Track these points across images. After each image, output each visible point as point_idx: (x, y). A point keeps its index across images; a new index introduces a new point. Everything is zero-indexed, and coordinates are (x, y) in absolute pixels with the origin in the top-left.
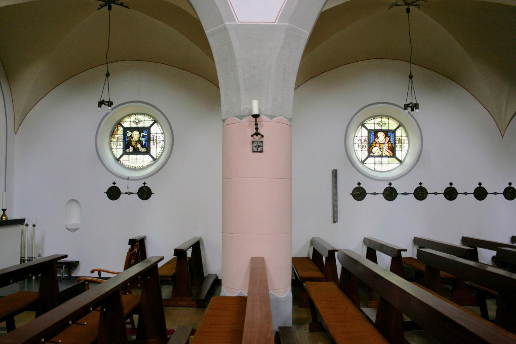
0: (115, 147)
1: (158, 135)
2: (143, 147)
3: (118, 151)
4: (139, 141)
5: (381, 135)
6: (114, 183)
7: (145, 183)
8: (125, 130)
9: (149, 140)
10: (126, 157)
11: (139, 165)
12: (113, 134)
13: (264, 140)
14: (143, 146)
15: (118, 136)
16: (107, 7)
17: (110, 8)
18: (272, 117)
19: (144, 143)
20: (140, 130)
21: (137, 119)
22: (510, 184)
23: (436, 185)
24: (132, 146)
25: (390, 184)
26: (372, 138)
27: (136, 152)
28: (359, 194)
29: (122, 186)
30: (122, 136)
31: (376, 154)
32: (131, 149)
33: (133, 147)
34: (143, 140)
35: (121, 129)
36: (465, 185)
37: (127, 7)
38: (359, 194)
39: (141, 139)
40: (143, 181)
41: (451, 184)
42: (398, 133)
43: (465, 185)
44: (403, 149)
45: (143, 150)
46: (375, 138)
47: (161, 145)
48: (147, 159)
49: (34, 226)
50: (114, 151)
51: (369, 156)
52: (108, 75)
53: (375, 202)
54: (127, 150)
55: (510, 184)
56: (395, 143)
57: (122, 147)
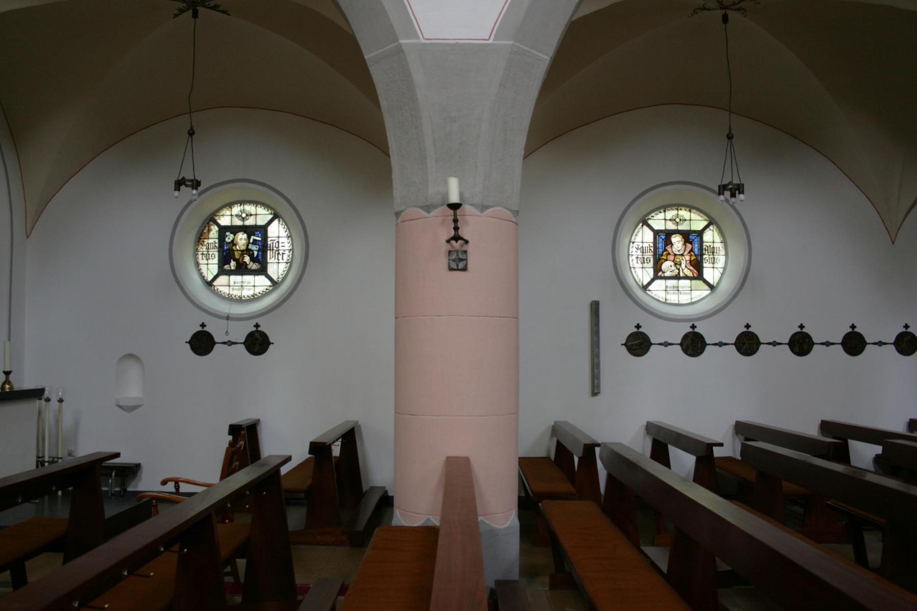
0: (205, 261)
1: (281, 240)
2: (254, 262)
3: (210, 268)
4: (248, 251)
5: (677, 240)
6: (203, 325)
7: (257, 326)
8: (223, 230)
9: (264, 247)
10: (223, 279)
11: (247, 293)
12: (200, 238)
13: (470, 248)
14: (253, 259)
15: (210, 241)
16: (191, 12)
17: (195, 15)
18: (483, 208)
19: (256, 253)
20: (249, 230)
21: (243, 211)
22: (906, 326)
23: (774, 329)
24: (235, 260)
25: (693, 327)
26: (661, 245)
27: (242, 269)
28: (638, 344)
29: (217, 331)
30: (217, 241)
31: (667, 274)
32: (233, 264)
33: (236, 260)
34: (254, 248)
35: (215, 229)
36: (827, 329)
37: (225, 12)
38: (638, 344)
39: (250, 246)
40: (254, 322)
41: (802, 327)
42: (708, 236)
43: (827, 329)
44: (715, 265)
45: (254, 266)
46: (666, 245)
47: (285, 257)
48: (261, 282)
49: (61, 401)
50: (204, 268)
51: (656, 277)
52: (191, 133)
53: (666, 359)
54: (226, 267)
55: (906, 326)
56: (702, 255)
57: (216, 261)
